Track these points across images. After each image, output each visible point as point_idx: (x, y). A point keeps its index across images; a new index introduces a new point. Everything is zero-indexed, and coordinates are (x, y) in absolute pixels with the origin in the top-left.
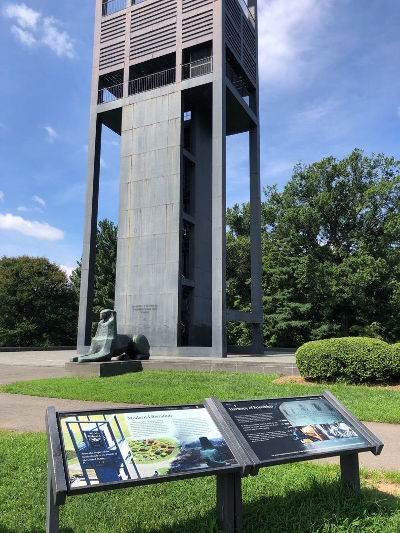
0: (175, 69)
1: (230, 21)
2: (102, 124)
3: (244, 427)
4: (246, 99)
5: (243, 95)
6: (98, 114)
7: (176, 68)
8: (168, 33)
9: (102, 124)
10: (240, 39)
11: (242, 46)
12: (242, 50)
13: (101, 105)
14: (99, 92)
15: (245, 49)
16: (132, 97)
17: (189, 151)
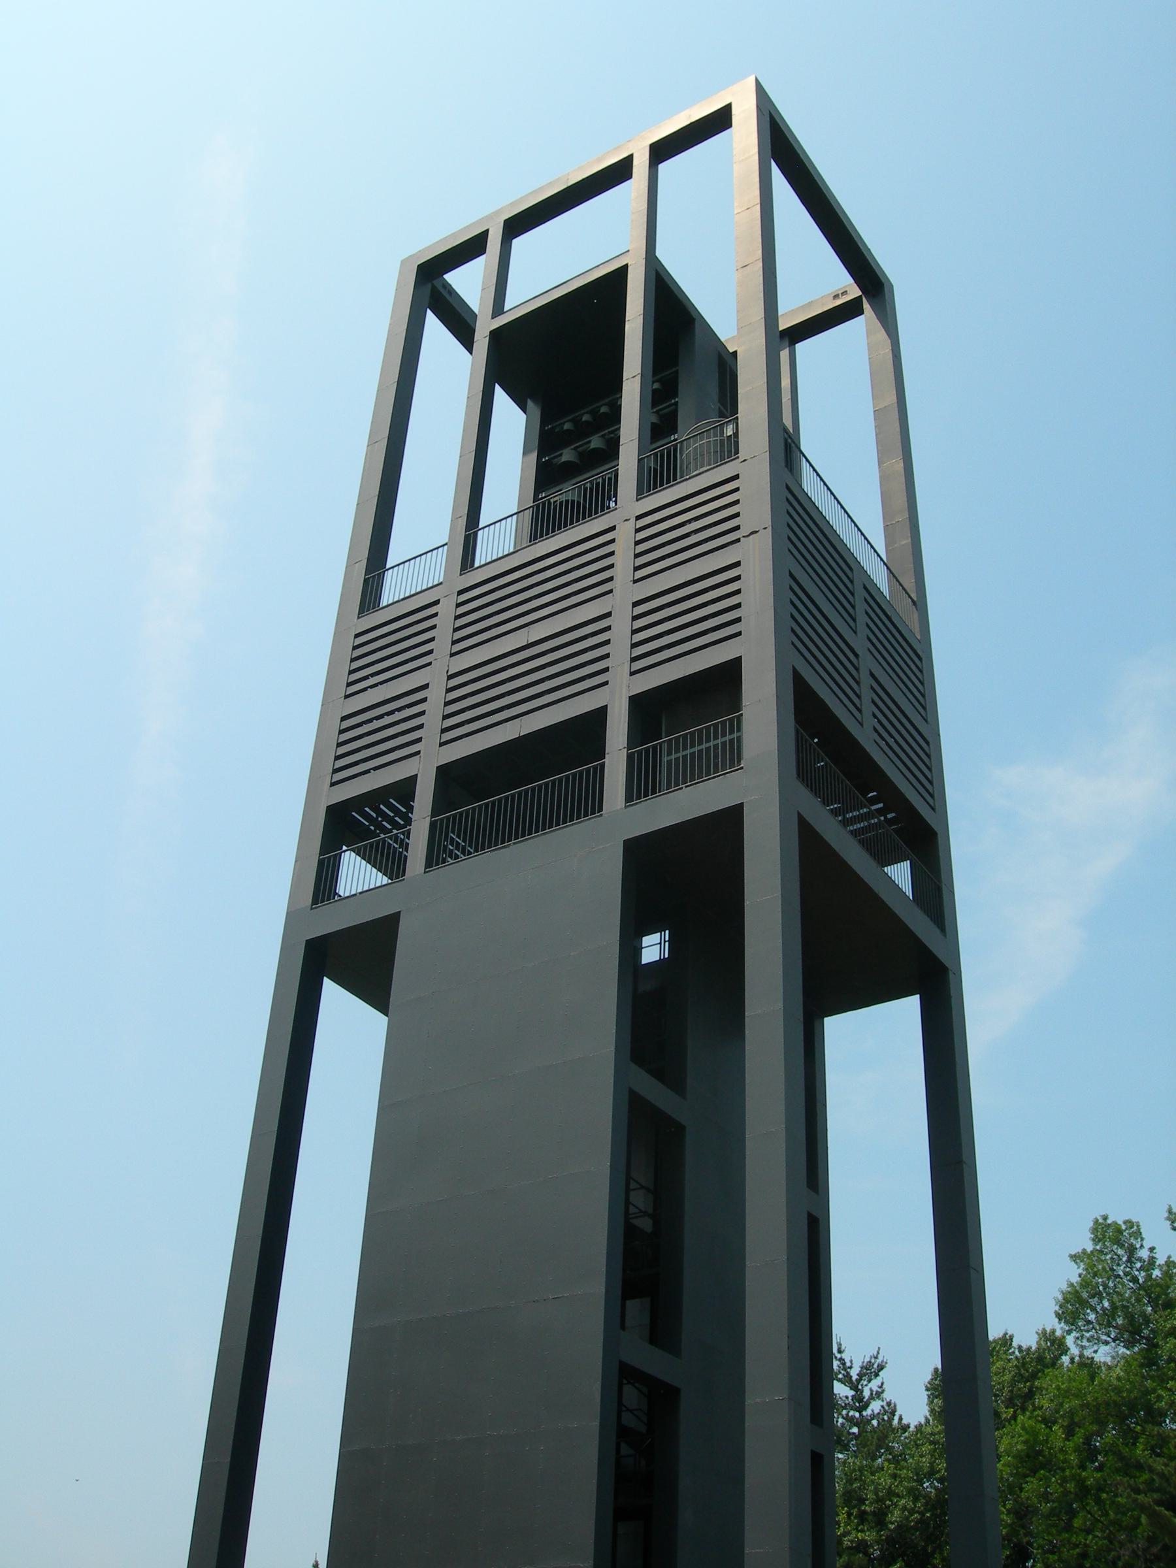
0: (603, 766)
1: (804, 509)
2: (326, 980)
3: (880, 812)
4: (901, 874)
5: (888, 857)
6: (309, 943)
7: (607, 760)
8: (584, 652)
9: (326, 980)
10: (856, 656)
11: (866, 681)
12: (867, 695)
13: (325, 909)
14: (321, 863)
15: (869, 599)
16: (444, 873)
17: (659, 1074)
